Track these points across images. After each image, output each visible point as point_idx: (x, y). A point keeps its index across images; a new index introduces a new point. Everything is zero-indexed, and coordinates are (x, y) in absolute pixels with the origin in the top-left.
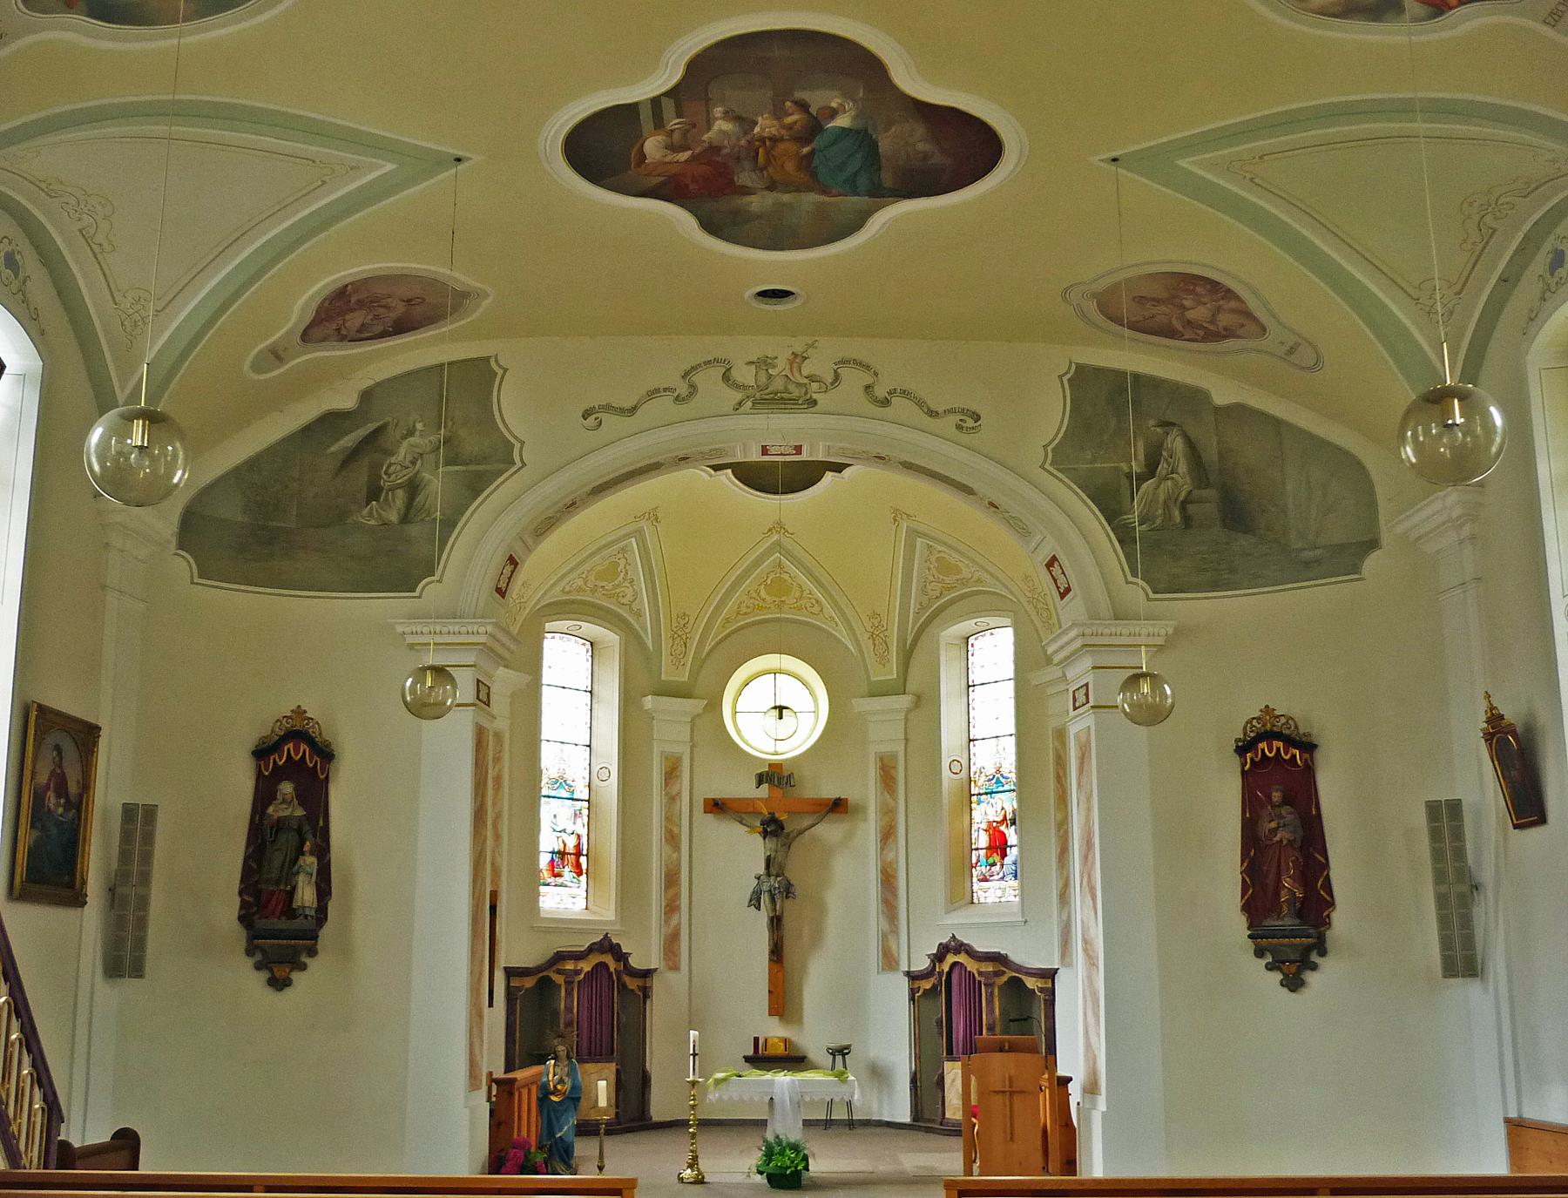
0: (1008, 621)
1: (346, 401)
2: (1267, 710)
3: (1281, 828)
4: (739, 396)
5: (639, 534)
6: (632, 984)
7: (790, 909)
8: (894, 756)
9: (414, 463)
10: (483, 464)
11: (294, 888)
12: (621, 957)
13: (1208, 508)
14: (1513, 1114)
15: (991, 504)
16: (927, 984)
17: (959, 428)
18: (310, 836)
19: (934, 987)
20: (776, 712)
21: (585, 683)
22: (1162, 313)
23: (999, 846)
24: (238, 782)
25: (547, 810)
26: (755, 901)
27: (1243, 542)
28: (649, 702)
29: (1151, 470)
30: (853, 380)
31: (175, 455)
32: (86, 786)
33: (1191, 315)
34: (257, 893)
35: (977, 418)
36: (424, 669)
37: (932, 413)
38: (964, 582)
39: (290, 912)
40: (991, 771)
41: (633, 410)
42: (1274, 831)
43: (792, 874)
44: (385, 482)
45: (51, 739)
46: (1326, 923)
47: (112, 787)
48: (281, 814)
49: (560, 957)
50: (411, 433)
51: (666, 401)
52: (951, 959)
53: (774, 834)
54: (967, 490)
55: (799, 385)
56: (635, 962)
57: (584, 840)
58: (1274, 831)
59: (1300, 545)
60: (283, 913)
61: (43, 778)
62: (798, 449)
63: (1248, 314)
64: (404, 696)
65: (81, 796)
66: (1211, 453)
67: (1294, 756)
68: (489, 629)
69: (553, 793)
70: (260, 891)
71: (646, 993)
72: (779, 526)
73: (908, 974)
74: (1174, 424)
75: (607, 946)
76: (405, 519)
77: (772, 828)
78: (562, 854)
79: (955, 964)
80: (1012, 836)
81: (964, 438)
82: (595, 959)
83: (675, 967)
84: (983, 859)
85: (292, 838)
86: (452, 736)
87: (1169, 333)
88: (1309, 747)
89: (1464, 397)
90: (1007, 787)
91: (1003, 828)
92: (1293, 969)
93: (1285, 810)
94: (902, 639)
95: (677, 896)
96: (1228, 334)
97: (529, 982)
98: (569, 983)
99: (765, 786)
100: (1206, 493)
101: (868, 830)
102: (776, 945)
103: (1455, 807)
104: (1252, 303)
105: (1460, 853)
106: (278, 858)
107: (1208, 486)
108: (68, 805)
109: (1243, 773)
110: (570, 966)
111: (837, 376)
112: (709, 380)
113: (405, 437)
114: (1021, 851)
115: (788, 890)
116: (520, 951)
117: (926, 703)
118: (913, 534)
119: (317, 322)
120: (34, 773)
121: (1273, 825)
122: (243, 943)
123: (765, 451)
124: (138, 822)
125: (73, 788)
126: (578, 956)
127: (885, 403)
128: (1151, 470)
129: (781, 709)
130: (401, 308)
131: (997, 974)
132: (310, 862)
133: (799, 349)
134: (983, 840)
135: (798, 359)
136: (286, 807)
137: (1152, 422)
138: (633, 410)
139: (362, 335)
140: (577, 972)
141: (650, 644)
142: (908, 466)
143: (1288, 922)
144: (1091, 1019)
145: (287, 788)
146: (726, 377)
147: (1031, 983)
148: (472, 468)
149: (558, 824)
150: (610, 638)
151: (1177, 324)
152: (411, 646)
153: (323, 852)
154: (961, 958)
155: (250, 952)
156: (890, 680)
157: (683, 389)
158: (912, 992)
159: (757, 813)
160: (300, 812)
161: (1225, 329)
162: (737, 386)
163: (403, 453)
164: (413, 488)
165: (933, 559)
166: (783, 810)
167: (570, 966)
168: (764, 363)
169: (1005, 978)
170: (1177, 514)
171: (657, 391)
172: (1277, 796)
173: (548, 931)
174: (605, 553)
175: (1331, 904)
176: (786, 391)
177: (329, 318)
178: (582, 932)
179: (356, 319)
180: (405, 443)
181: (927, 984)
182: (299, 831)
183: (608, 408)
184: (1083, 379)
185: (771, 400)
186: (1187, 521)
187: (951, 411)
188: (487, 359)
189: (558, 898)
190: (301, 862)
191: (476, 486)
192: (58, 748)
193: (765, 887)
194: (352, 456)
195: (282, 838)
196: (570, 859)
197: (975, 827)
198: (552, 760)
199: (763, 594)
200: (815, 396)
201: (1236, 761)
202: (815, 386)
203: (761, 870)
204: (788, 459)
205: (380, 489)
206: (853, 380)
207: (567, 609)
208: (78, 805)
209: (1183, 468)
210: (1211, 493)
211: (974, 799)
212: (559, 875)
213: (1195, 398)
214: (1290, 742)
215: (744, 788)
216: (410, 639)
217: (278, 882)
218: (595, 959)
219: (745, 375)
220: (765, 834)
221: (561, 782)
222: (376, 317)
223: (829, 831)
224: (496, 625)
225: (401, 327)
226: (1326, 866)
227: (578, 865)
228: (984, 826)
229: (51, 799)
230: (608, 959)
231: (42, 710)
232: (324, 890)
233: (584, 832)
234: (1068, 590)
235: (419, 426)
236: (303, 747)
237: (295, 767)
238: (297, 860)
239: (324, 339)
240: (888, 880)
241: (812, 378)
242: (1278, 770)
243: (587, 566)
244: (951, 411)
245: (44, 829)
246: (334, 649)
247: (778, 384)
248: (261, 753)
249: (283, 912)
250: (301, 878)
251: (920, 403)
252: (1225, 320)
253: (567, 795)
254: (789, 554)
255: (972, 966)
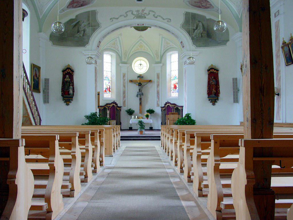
0: (177, 52)
1: (74, 17)
2: (212, 65)
3: (213, 82)
4: (134, 16)
5: (118, 37)
6: (118, 109)
7: (143, 97)
8: (159, 73)
9: (84, 27)
10: (95, 26)
11: (69, 91)
12: (116, 104)
13: (205, 35)
14: (241, 121)
15: (173, 33)
16: (164, 109)
17: (168, 21)
18: (71, 83)
19: (165, 109)
20: (140, 66)
21: (110, 62)
22: (199, 4)
23: (175, 87)
24: (60, 76)
25: (105, 82)
26: (137, 96)
27: (210, 40)
28: (121, 65)
29: (197, 28)
30: (152, 14)
31: (54, 28)
32: (39, 76)
33: (203, 5)
34: (64, 92)
35: (170, 20)
36: (89, 57)
37: (164, 19)
38: (171, 46)
39: (69, 94)
40: (174, 76)
41: (118, 19)
42: (212, 83)
43: (143, 92)
44: (80, 30)
45: (35, 68)
46: (219, 96)
47: (43, 76)
48: (67, 80)
49: (107, 104)
50: (84, 22)
51: (123, 17)
52: (167, 104)
53: (140, 85)
54: (169, 31)
55: (143, 14)
56: (119, 105)
57: (110, 87)
58: (212, 83)
59: (218, 40)
60: (68, 95)
61: (34, 75)
62: (143, 25)
63: (211, 5)
64: (86, 61)
65: (39, 78)
66: (206, 26)
67: (215, 72)
68: (97, 52)
69: (105, 79)
70: (64, 91)
71: (120, 110)
72: (141, 36)
73: (161, 107)
74: (200, 21)
75: (114, 103)
76: (83, 36)
77: (140, 84)
78: (107, 89)
79: (168, 105)
80: (177, 86)
81: (168, 23)
82: (113, 104)
83: (125, 106)
84: (173, 89)
85: (69, 84)
86: (92, 67)
87: (200, 7)
88: (218, 71)
89: (222, 22)
90: (177, 78)
91: (176, 85)
92: (214, 102)
93: (214, 80)
94: (161, 55)
95: (125, 95)
96: (208, 8)
97: (102, 108)
98: (108, 108)
99: (139, 78)
100: (205, 32)
101: (155, 85)
102: (141, 103)
103: (236, 79)
104: (212, 3)
105: (237, 86)
106: (66, 87)
107: (205, 31)
108: (37, 79)
109: (208, 74)
110: (109, 105)
111: (149, 13)
112: (129, 14)
113: (83, 23)
114: (178, 89)
115: (142, 94)
116: (102, 104)
117: (164, 65)
118: (163, 37)
119: (69, 5)
120: (33, 73)
121: (212, 82)
122: (62, 98)
123: (138, 25)
124: (47, 81)
125: (38, 76)
126: (110, 104)
127: (156, 17)
128: (197, 28)
129: (141, 64)
130: (82, 3)
131: (174, 107)
132: (71, 87)
133: (143, 9)
134: (173, 86)
135: (143, 10)
136: (68, 79)
137: (197, 21)
138: (118, 19)
139: (76, 7)
140: (110, 107)
141: (120, 55)
142: (160, 27)
143: (213, 95)
144: (185, 110)
145: (67, 76)
146: (132, 13)
147: (179, 108)
148: (93, 27)
149: (106, 84)
150: (114, 54)
151: (201, 6)
152: (85, 55)
153: (73, 86)
154: (169, 104)
155: (63, 100)
156: (158, 61)
157: (125, 15)
158: (162, 110)
159: (137, 82)
160: (69, 80)
161: (208, 7)
162: (134, 15)
163: (83, 25)
164: (84, 31)
165: (166, 42)
166: (142, 82)
167: (109, 105)
168: (138, 11)
169: (175, 107)
170: (200, 35)
171: (121, 15)
172: (213, 77)
173: (105, 100)
174: (113, 41)
175: (219, 93)
176: (141, 15)
177: (71, 4)
178: (110, 101)
179: (75, 5)
180: (83, 24)
181: (164, 109)
182: (70, 82)
183: (114, 18)
184: (187, 14)
185: (139, 17)
186: (202, 36)
187: (166, 19)
188: (95, 10)
189: (106, 95)
190: (70, 87)
191: (94, 30)
192: (36, 70)
193: (139, 94)
194: (75, 26)
195: (67, 84)
196: (109, 89)
197: (172, 84)
198: (105, 74)
199: (139, 47)
200: (146, 16)
201: (207, 73)
202: (146, 15)
203: (138, 91)
204: (142, 26)
205: (79, 31)
206: (152, 14)
207: (107, 50)
208: (38, 78)
209: (201, 28)
210: (206, 32)
211: (172, 80)
212: (107, 92)
213: (204, 17)
214: (215, 70)
215: (135, 78)
216: (85, 54)
217: (67, 90)
218: (113, 104)
219: (135, 13)
220: (139, 85)
221: (107, 77)
222: (78, 4)
223: (149, 85)
224: (98, 52)
225: (82, 6)
226: (219, 88)
227: (110, 90)
228: (173, 84)
229: (35, 77)
230: (114, 105)
231: (33, 64)
232: (73, 91)
233: (110, 85)
234: (184, 47)
235: (85, 21)
236: (70, 70)
237: (68, 74)
238: (69, 87)
239: (70, 7)
240: (158, 93)
241: (145, 13)
242: (213, 74)
243: (111, 43)
244: (166, 19)
245: (35, 82)
246: (74, 56)
247: (140, 14)
248: (63, 71)
249: (68, 93)
250: (70, 89)
251: (162, 18)
252: (208, 6)
253: (108, 79)
254: (143, 41)
255: (170, 105)
